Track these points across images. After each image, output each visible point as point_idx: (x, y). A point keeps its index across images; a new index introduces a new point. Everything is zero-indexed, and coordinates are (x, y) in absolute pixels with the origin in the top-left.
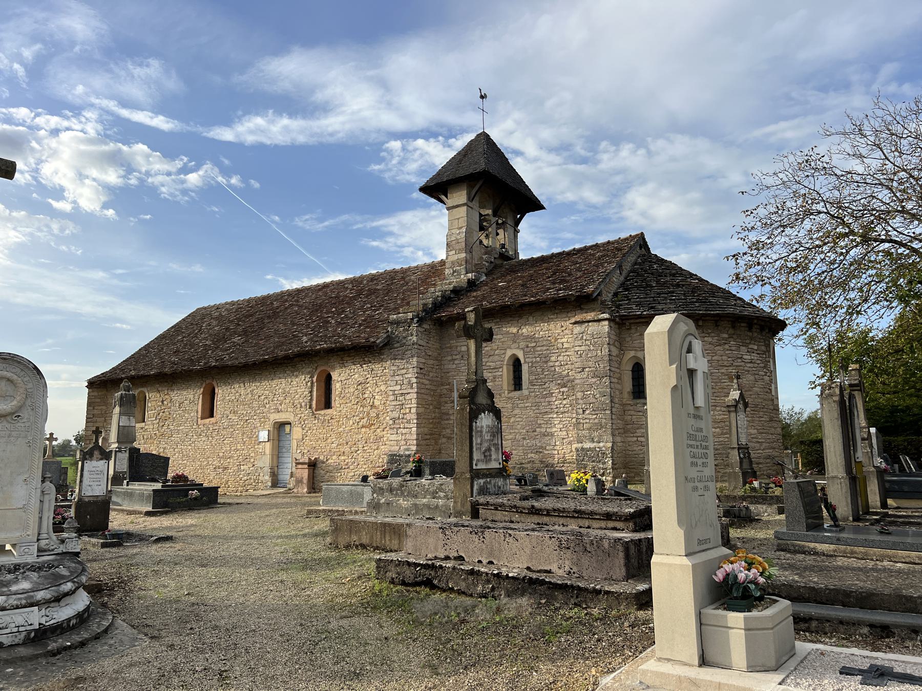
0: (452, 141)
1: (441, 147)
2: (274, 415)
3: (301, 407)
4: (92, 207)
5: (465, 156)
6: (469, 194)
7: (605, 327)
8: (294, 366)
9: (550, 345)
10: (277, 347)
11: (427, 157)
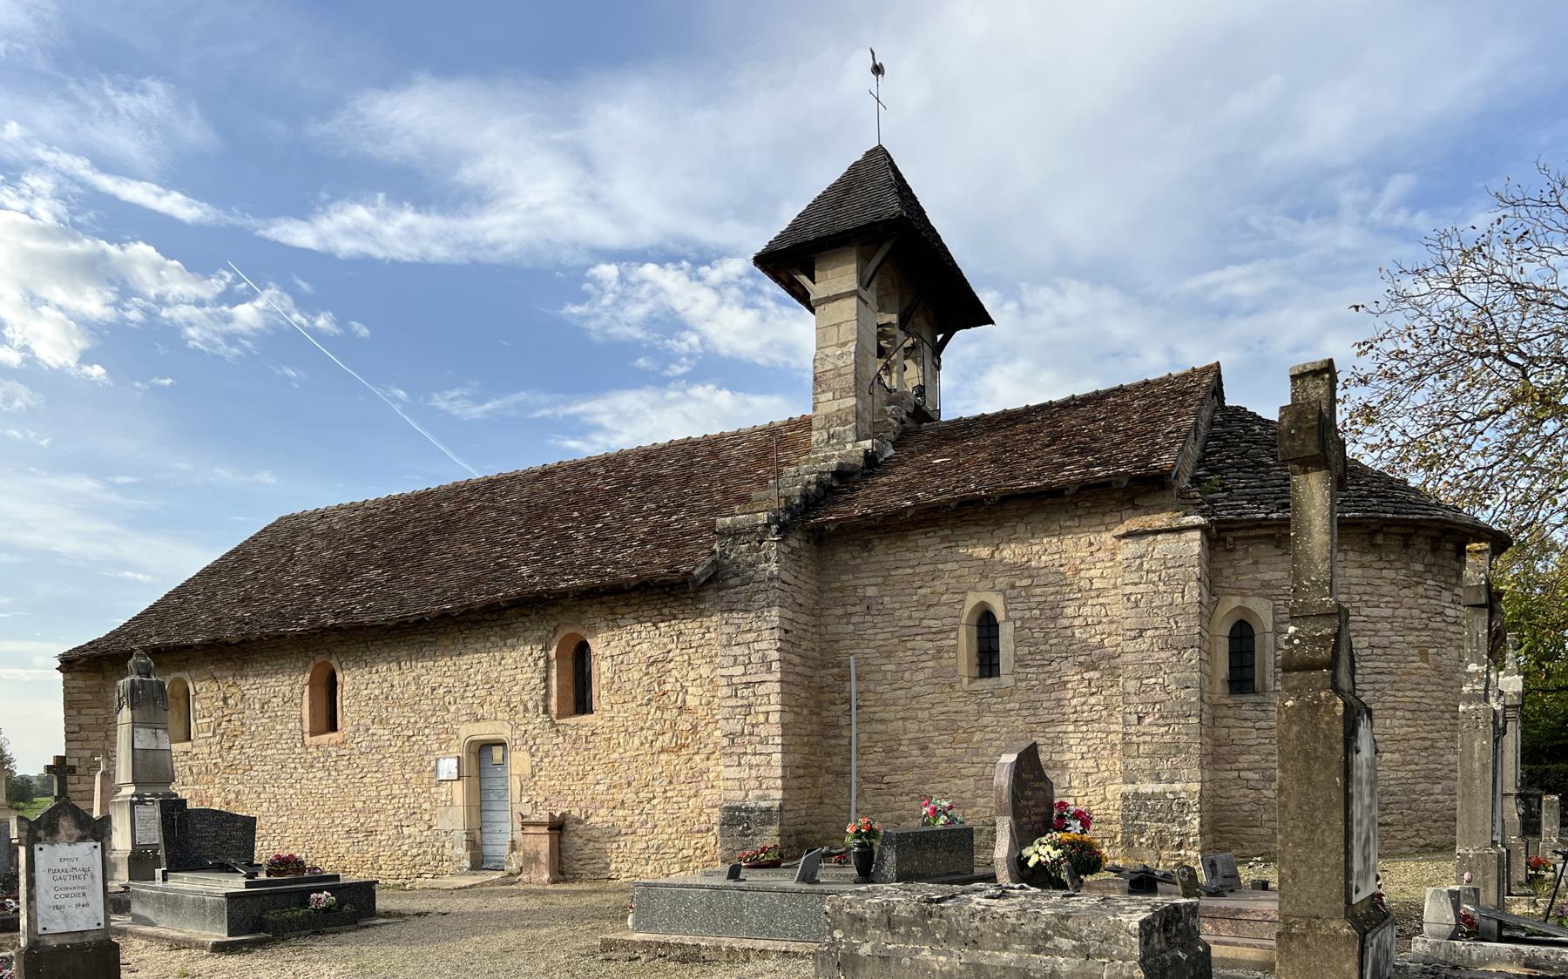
0: (704, 270)
1: (684, 279)
2: (468, 725)
3: (526, 710)
4: (61, 361)
5: (847, 192)
6: (861, 273)
7: (1193, 543)
8: (506, 626)
9: (1061, 582)
10: (468, 586)
11: (662, 295)
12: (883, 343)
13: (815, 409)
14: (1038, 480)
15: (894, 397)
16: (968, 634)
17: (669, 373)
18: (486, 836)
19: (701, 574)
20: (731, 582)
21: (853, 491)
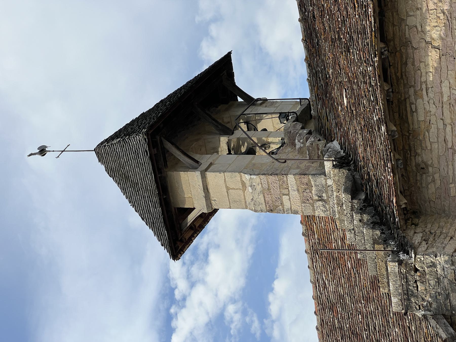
0: (178, 295)
1: (184, 311)
5: (127, 178)
12: (243, 150)
13: (296, 212)
14: (367, 6)
15: (288, 141)
17: (258, 335)
19: (446, 331)
21: (369, 180)
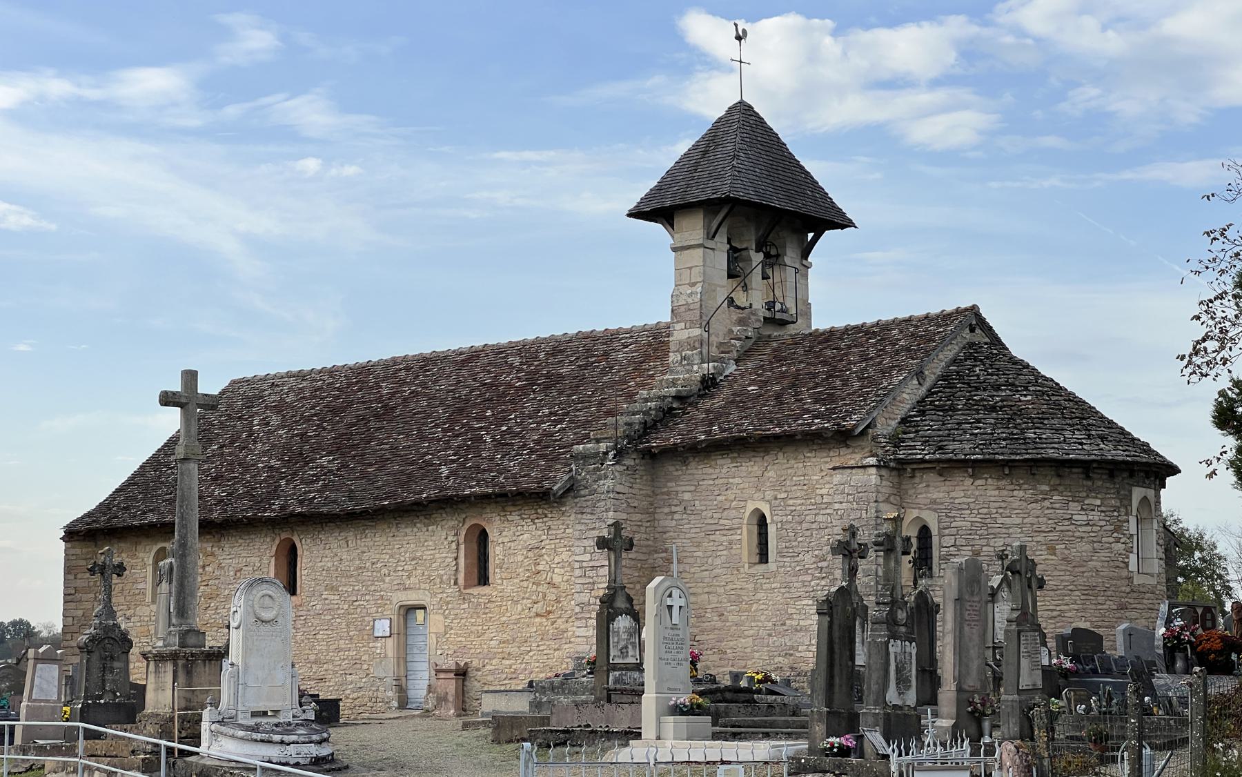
2: (399, 593)
6: (707, 227)
8: (428, 516)
10: (400, 484)
16: (749, 532)
18: (410, 682)
19: (559, 489)
20: (582, 493)
